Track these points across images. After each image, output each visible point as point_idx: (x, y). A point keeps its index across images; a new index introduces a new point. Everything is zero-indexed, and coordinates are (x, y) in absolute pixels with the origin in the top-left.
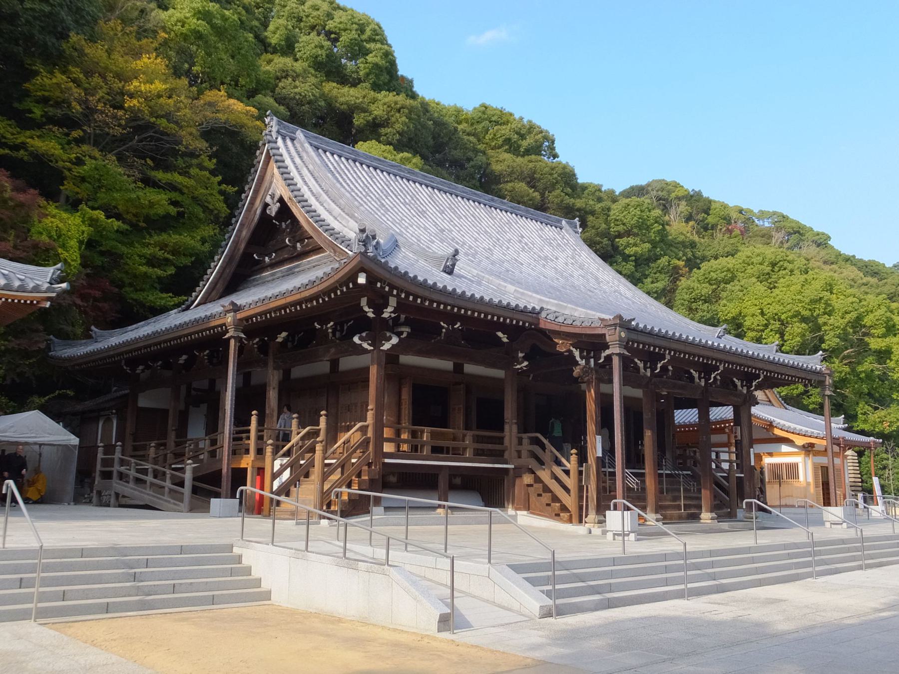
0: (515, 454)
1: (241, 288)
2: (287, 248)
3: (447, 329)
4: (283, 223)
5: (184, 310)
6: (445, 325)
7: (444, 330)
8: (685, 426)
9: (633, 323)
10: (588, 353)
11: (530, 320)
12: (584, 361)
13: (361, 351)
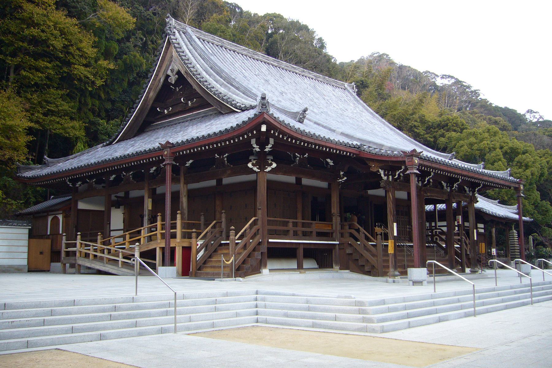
0: (339, 235)
1: (147, 130)
2: (181, 104)
3: (300, 158)
4: (177, 88)
5: (107, 145)
6: (299, 155)
7: (298, 158)
8: (133, 198)
9: (421, 154)
10: (388, 172)
11: (355, 152)
12: (386, 177)
13: (252, 171)
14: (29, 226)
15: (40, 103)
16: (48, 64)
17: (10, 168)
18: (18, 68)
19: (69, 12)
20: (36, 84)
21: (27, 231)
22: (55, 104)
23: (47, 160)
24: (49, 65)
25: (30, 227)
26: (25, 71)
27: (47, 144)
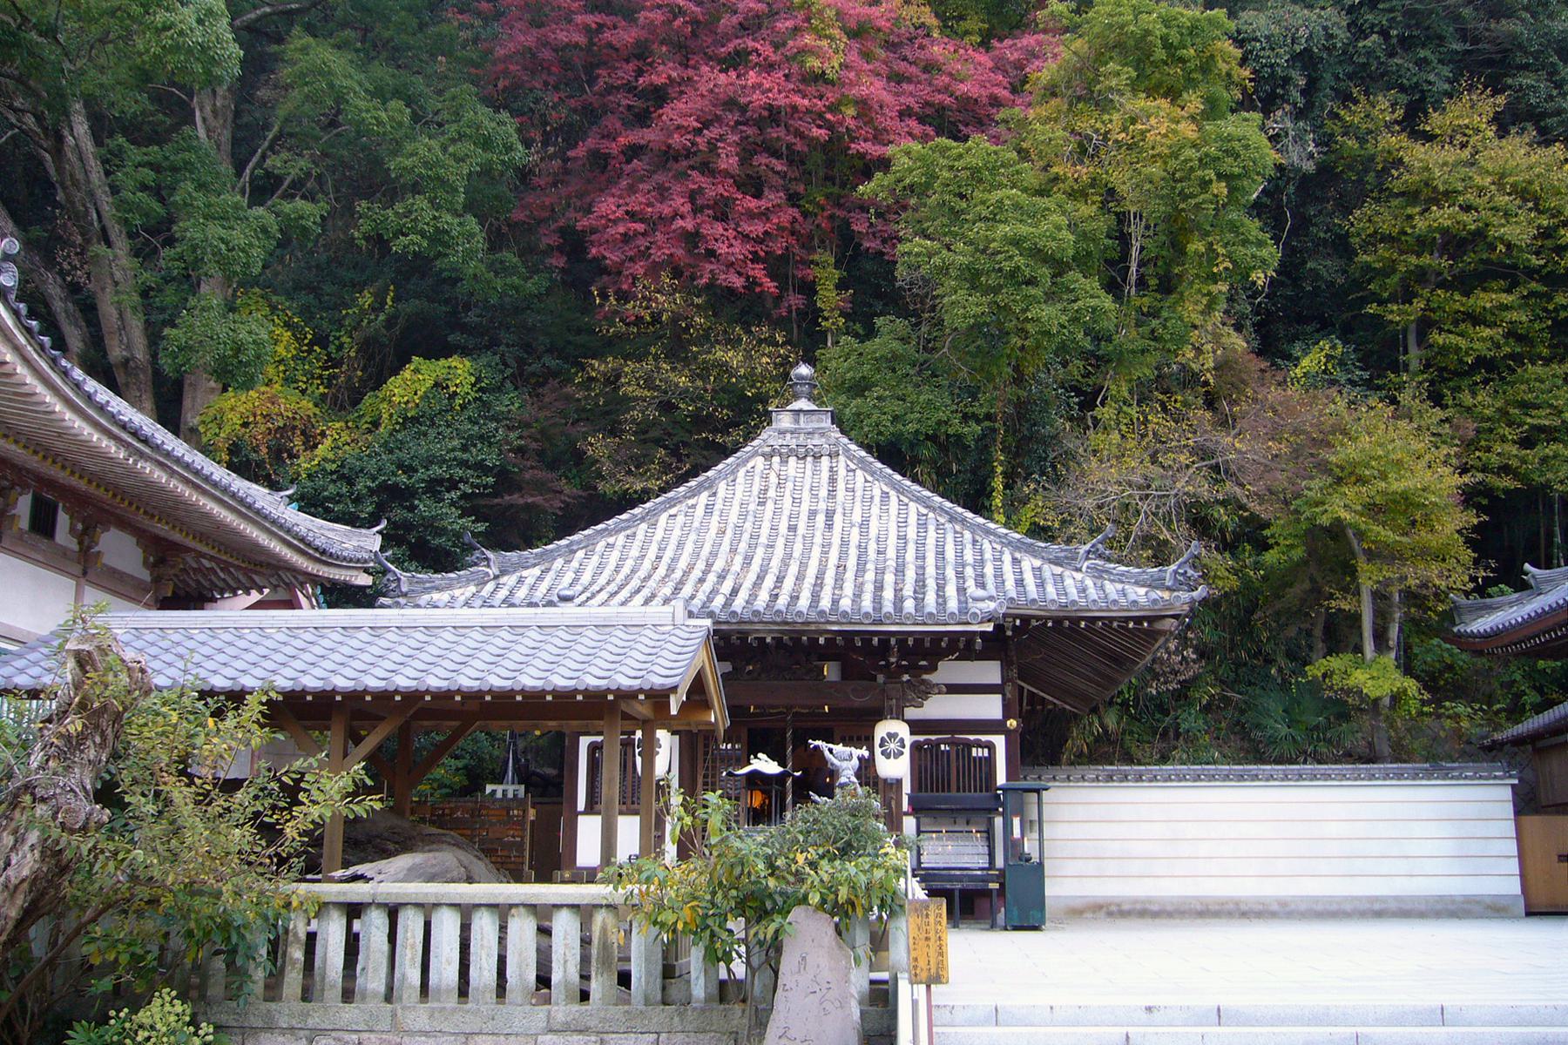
14: (1511, 777)
15: (1503, 412)
16: (1504, 295)
17: (1435, 612)
18: (1425, 325)
19: (1542, 131)
20: (1482, 362)
21: (1507, 793)
22: (1551, 406)
23: (1533, 576)
24: (1507, 299)
25: (1516, 782)
26: (1441, 330)
27: (1557, 529)
